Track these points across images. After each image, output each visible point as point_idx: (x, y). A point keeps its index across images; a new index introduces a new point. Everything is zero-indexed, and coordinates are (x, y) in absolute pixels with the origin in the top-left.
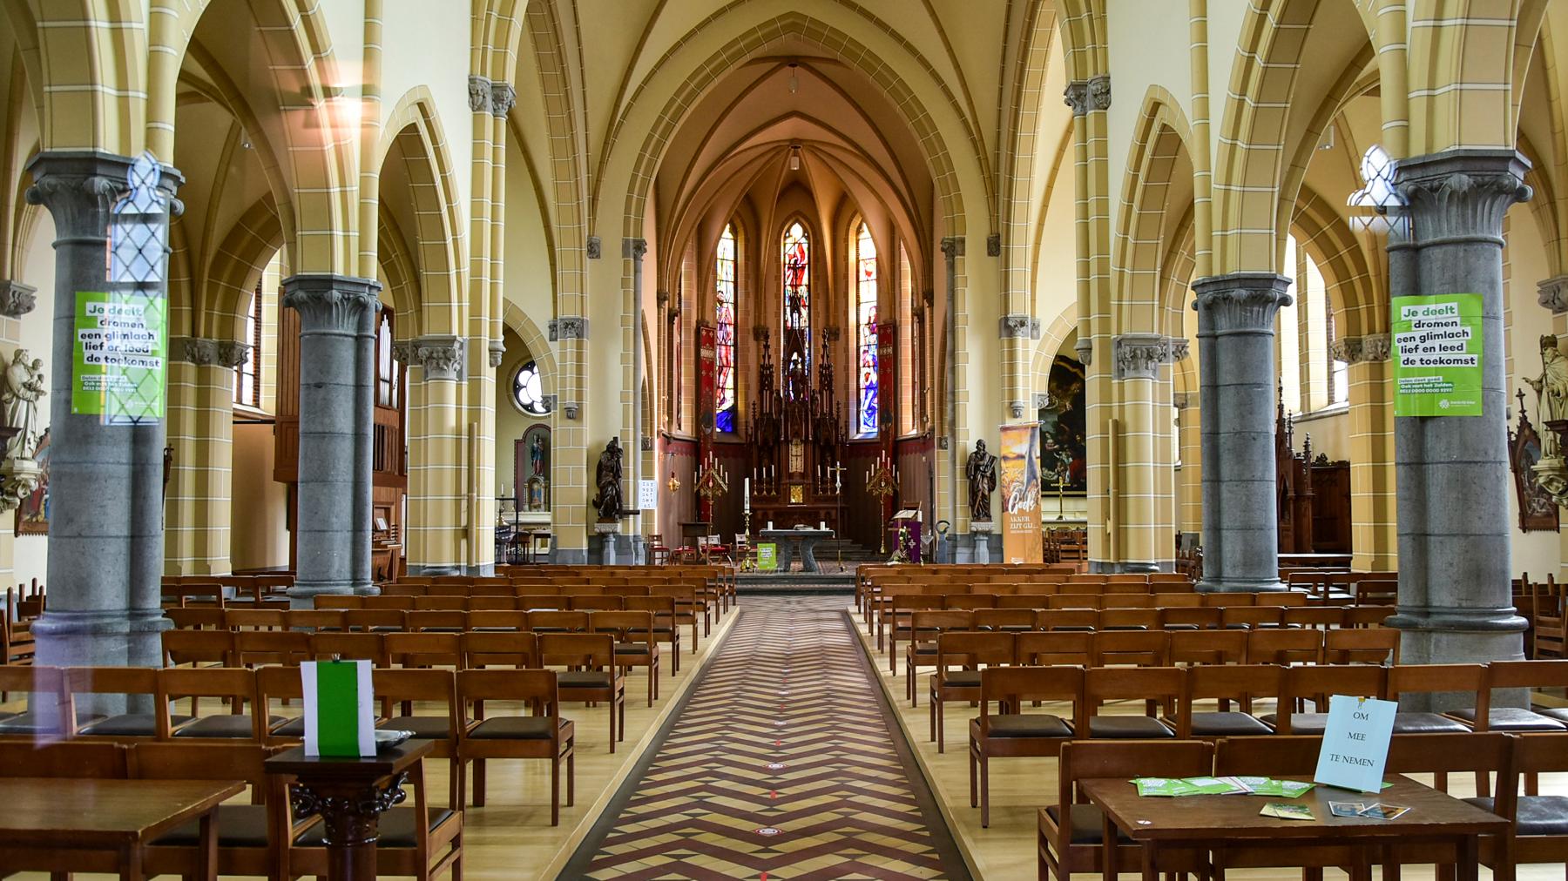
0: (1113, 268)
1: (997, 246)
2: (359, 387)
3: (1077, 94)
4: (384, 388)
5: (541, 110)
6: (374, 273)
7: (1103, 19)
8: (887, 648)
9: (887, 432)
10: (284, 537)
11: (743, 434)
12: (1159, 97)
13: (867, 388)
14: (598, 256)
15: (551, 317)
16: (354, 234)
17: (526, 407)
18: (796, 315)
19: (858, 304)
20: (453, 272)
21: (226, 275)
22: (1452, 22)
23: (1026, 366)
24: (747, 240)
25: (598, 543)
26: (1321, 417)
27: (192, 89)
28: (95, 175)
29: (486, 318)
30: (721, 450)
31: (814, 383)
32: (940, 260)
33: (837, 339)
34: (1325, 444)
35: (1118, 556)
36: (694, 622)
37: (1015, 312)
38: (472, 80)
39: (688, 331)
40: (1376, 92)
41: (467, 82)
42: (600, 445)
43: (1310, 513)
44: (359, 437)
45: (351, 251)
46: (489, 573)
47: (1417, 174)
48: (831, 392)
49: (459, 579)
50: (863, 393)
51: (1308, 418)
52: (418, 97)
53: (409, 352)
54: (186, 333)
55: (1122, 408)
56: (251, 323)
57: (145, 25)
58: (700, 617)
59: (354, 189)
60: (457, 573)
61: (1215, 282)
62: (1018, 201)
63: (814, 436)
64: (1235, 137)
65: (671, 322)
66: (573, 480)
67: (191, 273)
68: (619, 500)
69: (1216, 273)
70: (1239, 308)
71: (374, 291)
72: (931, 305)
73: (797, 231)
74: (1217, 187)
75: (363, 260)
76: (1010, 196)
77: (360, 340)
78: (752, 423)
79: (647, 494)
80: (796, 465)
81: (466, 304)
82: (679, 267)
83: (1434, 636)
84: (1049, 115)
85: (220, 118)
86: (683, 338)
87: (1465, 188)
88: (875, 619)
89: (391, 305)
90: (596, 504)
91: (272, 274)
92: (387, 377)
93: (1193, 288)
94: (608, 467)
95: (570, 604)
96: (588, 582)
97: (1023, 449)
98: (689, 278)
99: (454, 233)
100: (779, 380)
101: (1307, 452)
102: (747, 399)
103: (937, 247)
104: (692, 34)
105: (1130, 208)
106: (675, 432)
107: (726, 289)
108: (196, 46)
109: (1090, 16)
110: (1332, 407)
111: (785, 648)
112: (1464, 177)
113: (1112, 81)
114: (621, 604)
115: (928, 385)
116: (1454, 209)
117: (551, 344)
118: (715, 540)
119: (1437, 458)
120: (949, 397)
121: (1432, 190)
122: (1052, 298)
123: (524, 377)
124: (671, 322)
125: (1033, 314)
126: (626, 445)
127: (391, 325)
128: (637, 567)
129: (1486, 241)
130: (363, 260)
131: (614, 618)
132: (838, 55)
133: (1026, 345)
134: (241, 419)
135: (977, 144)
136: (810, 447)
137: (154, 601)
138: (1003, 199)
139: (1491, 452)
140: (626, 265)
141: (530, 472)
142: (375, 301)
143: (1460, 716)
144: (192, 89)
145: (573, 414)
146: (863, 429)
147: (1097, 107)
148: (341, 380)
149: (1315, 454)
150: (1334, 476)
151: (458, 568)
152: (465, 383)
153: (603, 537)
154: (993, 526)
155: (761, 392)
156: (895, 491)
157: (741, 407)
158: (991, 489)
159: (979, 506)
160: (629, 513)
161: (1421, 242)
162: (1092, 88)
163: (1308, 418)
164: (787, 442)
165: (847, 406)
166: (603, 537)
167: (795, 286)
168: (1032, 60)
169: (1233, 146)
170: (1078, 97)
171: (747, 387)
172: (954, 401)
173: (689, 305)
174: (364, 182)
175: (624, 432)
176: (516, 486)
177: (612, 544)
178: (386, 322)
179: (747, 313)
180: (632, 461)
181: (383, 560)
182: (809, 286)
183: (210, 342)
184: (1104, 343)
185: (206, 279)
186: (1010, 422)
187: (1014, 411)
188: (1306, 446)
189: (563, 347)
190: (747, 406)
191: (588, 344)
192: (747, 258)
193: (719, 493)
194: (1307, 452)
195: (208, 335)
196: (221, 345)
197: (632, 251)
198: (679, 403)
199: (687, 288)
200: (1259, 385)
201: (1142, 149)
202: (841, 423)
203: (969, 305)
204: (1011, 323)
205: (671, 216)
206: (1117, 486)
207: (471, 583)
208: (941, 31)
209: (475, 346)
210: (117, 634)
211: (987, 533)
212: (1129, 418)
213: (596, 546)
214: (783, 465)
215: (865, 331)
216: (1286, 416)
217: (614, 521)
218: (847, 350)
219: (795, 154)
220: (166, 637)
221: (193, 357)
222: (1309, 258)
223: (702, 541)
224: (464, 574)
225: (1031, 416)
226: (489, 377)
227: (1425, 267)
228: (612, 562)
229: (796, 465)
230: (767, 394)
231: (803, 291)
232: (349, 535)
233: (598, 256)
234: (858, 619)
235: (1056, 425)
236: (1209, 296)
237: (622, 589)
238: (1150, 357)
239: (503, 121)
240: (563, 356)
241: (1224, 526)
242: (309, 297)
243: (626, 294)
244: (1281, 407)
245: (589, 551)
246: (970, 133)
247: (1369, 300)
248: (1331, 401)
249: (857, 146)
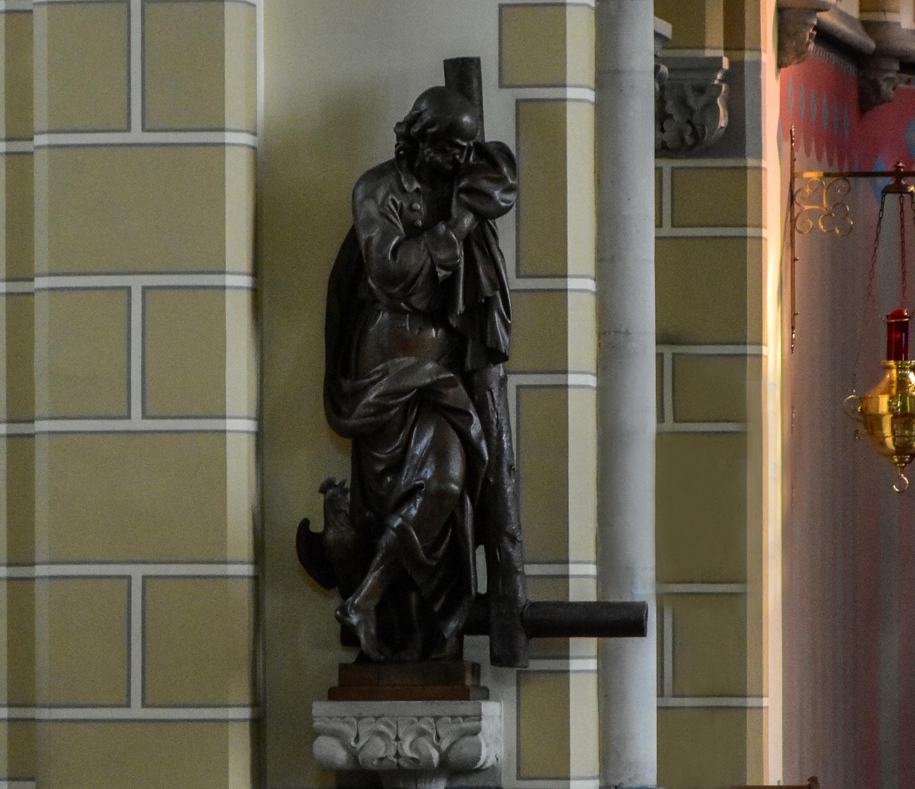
42: (343, 116)
68: (493, 527)
90: (324, 560)
126: (543, 119)
143: (852, 393)
160: (566, 622)
180: (590, 248)
217: (453, 683)
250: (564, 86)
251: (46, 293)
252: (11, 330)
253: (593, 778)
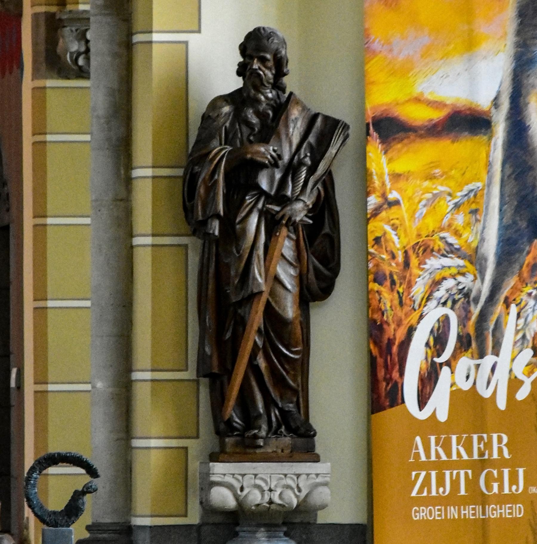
158: (317, 287)
228: (234, 301)
250: (151, 32)
251: (152, 436)
252: (44, 195)
253: (137, 178)
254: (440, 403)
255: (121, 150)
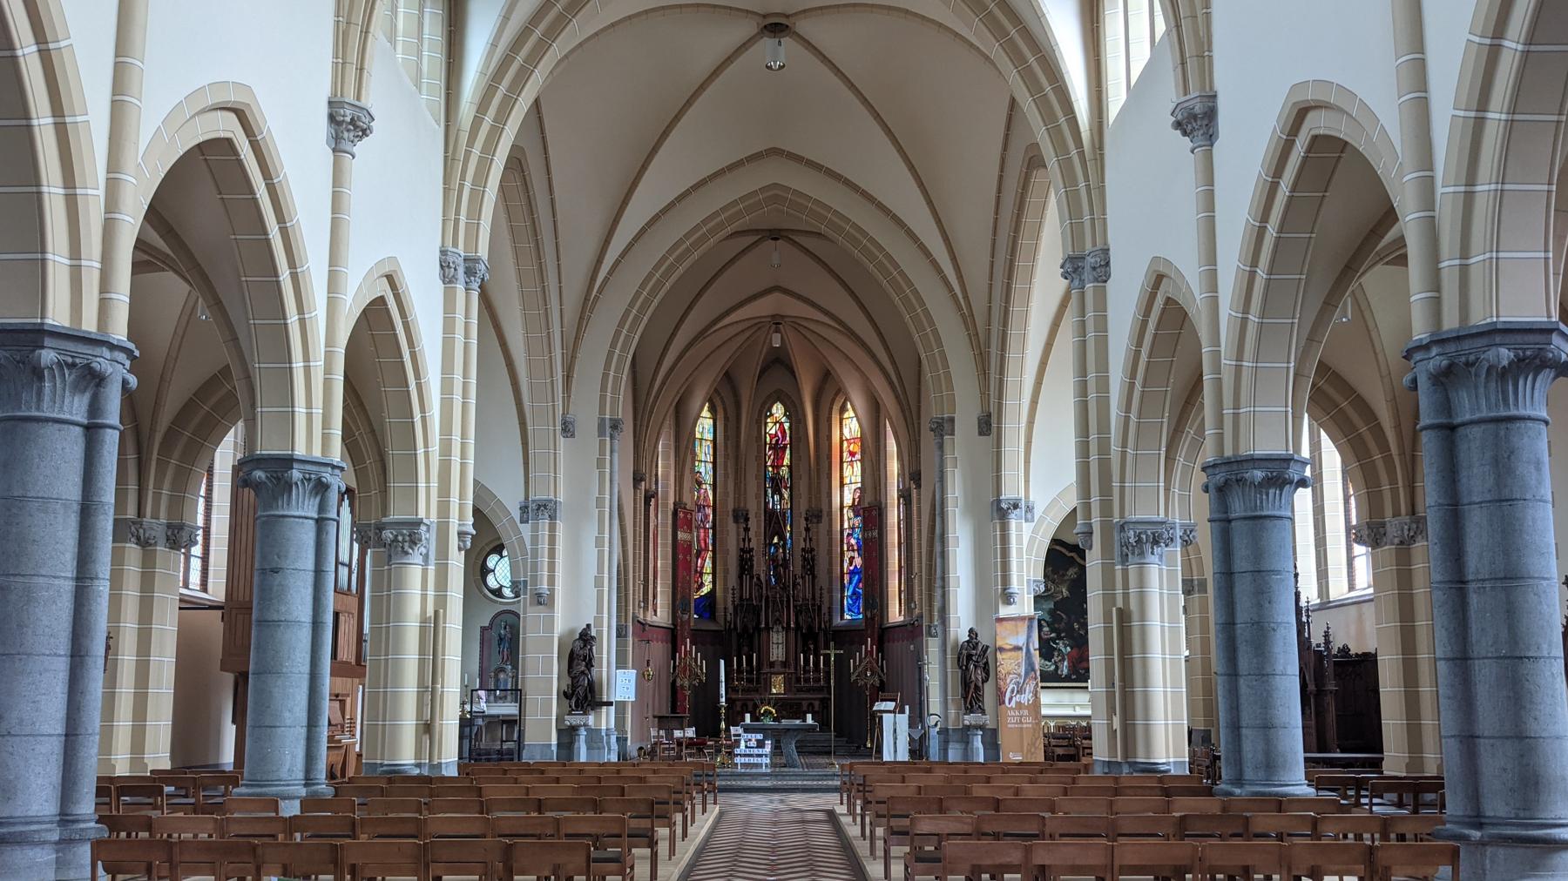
0: (1115, 448)
1: (988, 425)
2: (319, 572)
3: (1073, 267)
4: (344, 571)
5: (515, 284)
6: (337, 453)
7: (1102, 189)
8: (880, 853)
9: (873, 618)
10: (229, 732)
11: (722, 622)
12: (1161, 269)
13: (852, 573)
14: (573, 436)
15: (522, 498)
16: (318, 411)
17: (493, 592)
18: (776, 497)
19: (842, 485)
20: (421, 451)
21: (177, 454)
22: (1486, 187)
23: (1020, 550)
24: (726, 419)
25: (568, 736)
26: (1342, 605)
27: (146, 257)
28: (43, 347)
29: (455, 500)
30: (698, 637)
31: (796, 567)
32: (928, 439)
33: (819, 522)
34: (1353, 635)
35: (1126, 754)
36: (671, 825)
37: (1008, 494)
38: (443, 252)
39: (665, 513)
40: (1402, 260)
41: (438, 254)
42: (572, 632)
43: (1332, 708)
44: (316, 625)
45: (314, 428)
46: (453, 772)
47: (1451, 348)
48: (814, 577)
49: (420, 779)
50: (846, 578)
51: (1326, 605)
52: (387, 269)
53: (371, 534)
54: (131, 513)
55: (1126, 596)
56: (201, 501)
57: (101, 192)
58: (678, 817)
59: (318, 364)
60: (416, 772)
61: (1228, 463)
62: (1010, 380)
63: (797, 623)
64: (1246, 310)
65: (647, 504)
66: (544, 674)
67: (139, 450)
69: (1228, 453)
70: (1247, 494)
71: (337, 471)
72: (919, 486)
73: (778, 410)
74: (1227, 362)
75: (326, 438)
76: (1002, 373)
77: (320, 523)
78: (731, 609)
79: (622, 685)
80: (777, 653)
81: (434, 484)
82: (656, 447)
83: (1489, 850)
84: (1044, 286)
85: (173, 288)
86: (661, 520)
87: (1505, 363)
88: (859, 811)
89: (354, 485)
91: (226, 454)
92: (346, 560)
93: (1204, 469)
94: (579, 654)
95: (540, 806)
96: (557, 780)
97: (1021, 640)
98: (666, 458)
99: (423, 410)
100: (760, 566)
101: (1327, 642)
102: (725, 583)
103: (925, 426)
104: (671, 205)
105: (1132, 386)
106: (650, 618)
107: (705, 470)
108: (155, 215)
109: (1088, 186)
110: (1353, 594)
111: (765, 799)
112: (1504, 351)
113: (1112, 253)
114: (596, 806)
115: (916, 570)
116: (1493, 385)
117: (521, 526)
118: (690, 732)
119: (1483, 653)
120: (938, 583)
121: (1468, 364)
122: (1044, 478)
123: (492, 561)
124: (647, 504)
125: (1027, 496)
126: (600, 633)
127: (351, 505)
128: (609, 763)
129: (1530, 418)
130: (326, 438)
131: (584, 821)
132: (823, 229)
133: (1019, 529)
134: (188, 605)
135: (968, 320)
136: (792, 634)
137: (87, 805)
138: (994, 376)
139: (1545, 646)
140: (602, 444)
141: (497, 660)
142: (337, 482)
144: (146, 257)
145: (543, 601)
146: (847, 617)
147: (1096, 280)
148: (298, 565)
149: (1337, 645)
150: (1359, 669)
151: (418, 765)
152: (431, 568)
153: (574, 729)
154: (988, 720)
155: (740, 577)
156: (882, 682)
157: (719, 593)
158: (985, 680)
159: (971, 696)
161: (1458, 420)
162: (1090, 260)
163: (1326, 605)
164: (768, 629)
165: (830, 591)
166: (574, 729)
167: (777, 467)
168: (1025, 231)
169: (1244, 321)
170: (1075, 270)
171: (726, 571)
172: (943, 587)
173: (666, 486)
174: (329, 356)
175: (598, 620)
176: (481, 676)
177: (582, 738)
178: (346, 502)
179: (726, 494)
181: (337, 757)
182: (790, 467)
183: (155, 525)
184: (1106, 527)
185: (155, 456)
186: (1004, 611)
187: (1008, 598)
188: (1327, 635)
189: (535, 529)
190: (725, 590)
191: (560, 525)
192: (726, 438)
193: (696, 683)
194: (1327, 642)
195: (155, 516)
196: (169, 526)
197: (608, 430)
198: (655, 587)
199: (664, 466)
200: (1278, 572)
201: (1144, 324)
202: (825, 609)
203: (956, 491)
204: (1004, 506)
205: (648, 394)
206: (1123, 678)
207: (428, 785)
208: (930, 203)
209: (443, 529)
210: (45, 842)
211: (981, 727)
212: (1133, 606)
213: (566, 740)
214: (764, 652)
215: (848, 514)
216: (1303, 603)
218: (830, 532)
219: (777, 331)
220: (97, 846)
221: (138, 538)
222: (1323, 433)
223: (678, 734)
224: (426, 772)
225: (1024, 605)
226: (457, 561)
227: (1463, 447)
228: (583, 759)
229: (777, 653)
230: (746, 578)
231: (784, 471)
232: (304, 731)
233: (573, 436)
234: (846, 820)
235: (1052, 613)
236: (1220, 478)
237: (599, 788)
238: (1156, 542)
239: (475, 295)
240: (535, 540)
241: (1243, 723)
242: (265, 480)
243: (602, 475)
244: (1297, 595)
245: (559, 745)
246: (960, 308)
247: (1393, 481)
248: (1351, 587)
249: (840, 322)
254: (1013, 704)
255: (945, 652)
